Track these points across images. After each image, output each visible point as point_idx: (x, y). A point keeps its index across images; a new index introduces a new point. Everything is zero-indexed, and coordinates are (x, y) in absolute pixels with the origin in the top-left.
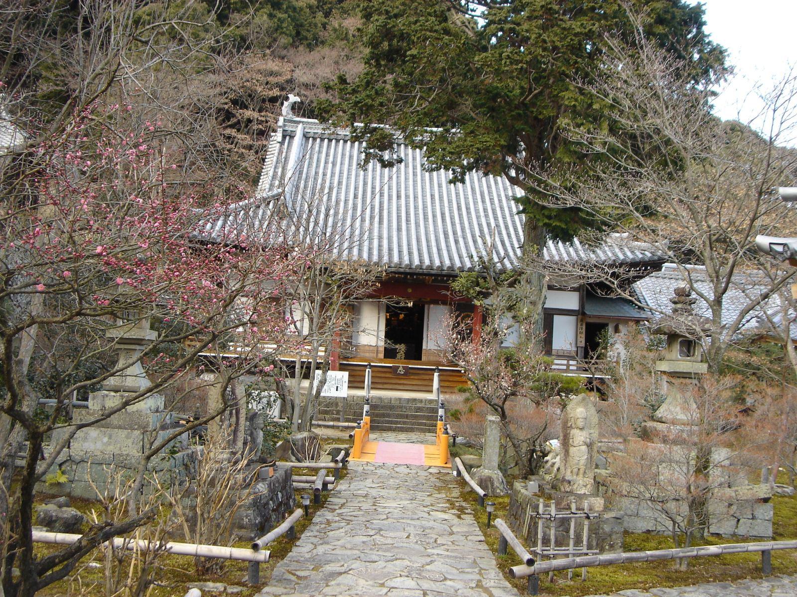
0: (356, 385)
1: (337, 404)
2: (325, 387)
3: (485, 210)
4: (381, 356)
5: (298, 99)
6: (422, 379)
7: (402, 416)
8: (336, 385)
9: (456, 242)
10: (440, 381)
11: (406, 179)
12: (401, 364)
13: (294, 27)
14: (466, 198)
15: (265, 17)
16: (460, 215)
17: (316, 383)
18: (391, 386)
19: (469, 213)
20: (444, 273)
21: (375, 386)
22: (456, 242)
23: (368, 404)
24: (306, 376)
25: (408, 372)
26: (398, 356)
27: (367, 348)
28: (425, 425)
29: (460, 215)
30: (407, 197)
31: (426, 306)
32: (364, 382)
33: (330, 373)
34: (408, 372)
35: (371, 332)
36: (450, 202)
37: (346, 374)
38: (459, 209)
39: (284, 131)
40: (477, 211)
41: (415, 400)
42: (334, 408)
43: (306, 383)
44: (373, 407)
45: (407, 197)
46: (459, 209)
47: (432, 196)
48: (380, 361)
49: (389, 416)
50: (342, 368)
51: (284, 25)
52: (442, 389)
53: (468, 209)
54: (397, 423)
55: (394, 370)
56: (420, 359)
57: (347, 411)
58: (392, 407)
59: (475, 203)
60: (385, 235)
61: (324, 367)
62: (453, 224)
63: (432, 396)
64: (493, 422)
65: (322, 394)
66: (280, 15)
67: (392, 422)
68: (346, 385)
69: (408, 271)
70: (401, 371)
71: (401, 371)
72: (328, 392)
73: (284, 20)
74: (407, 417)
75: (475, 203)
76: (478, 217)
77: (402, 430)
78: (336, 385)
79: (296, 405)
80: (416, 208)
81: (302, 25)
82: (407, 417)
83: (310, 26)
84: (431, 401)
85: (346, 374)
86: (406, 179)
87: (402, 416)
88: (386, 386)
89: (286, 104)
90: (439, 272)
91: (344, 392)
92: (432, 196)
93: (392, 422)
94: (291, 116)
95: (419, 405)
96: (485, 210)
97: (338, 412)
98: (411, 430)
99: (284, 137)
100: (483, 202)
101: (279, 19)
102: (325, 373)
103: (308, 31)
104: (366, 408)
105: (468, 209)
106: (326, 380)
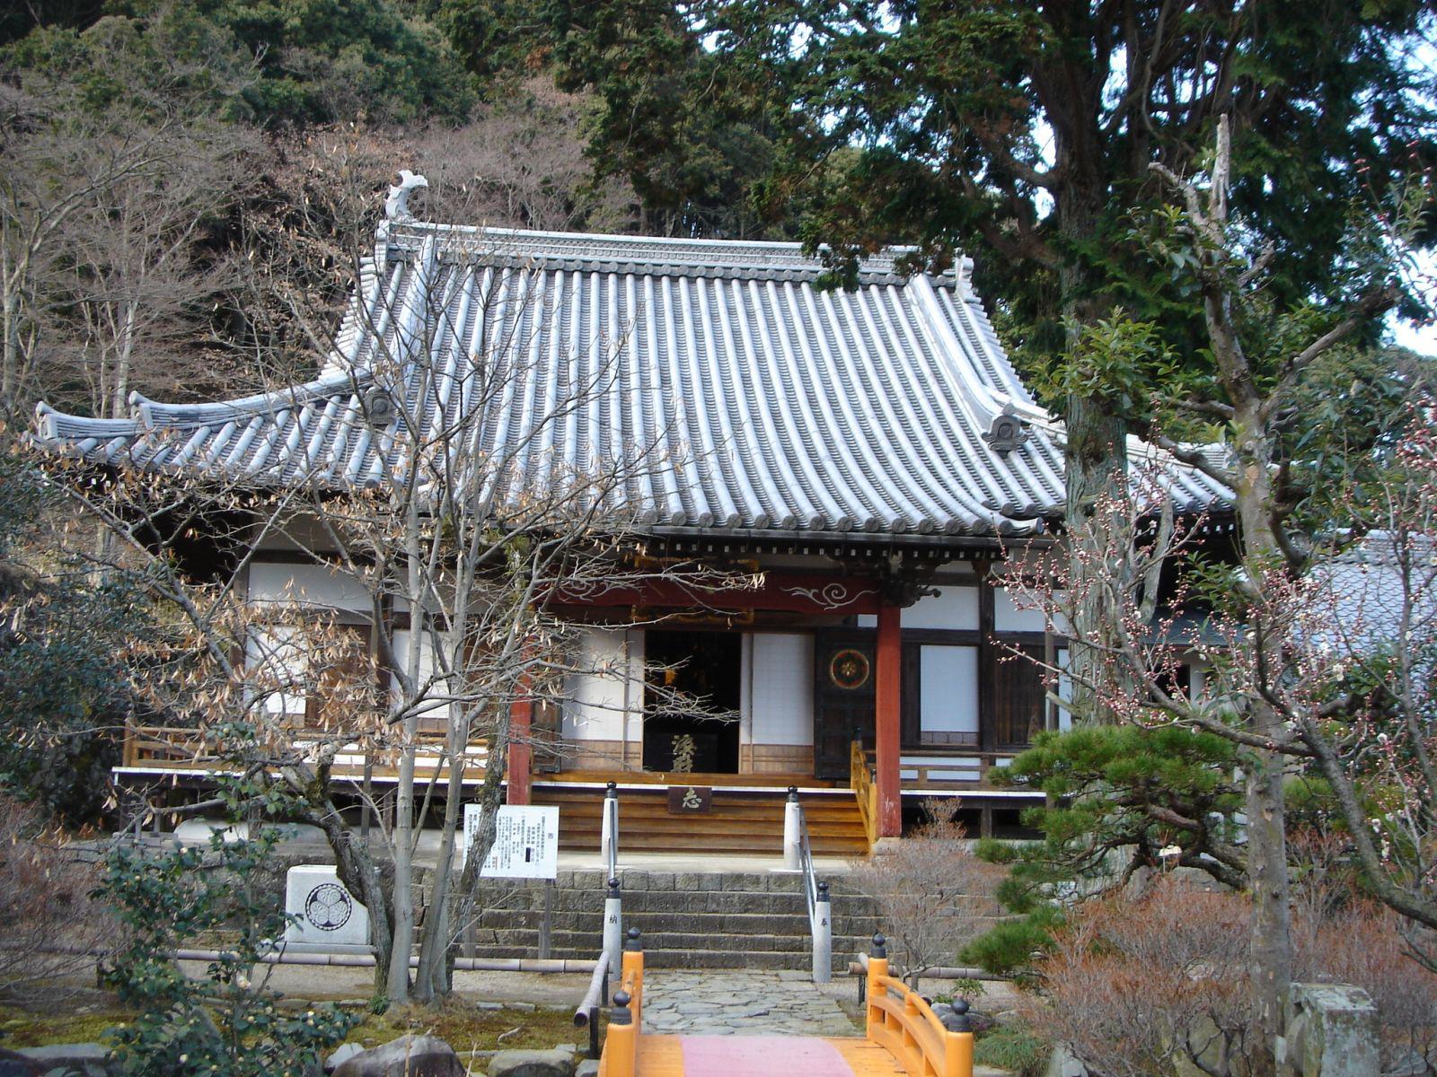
0: (577, 841)
1: (528, 901)
2: (495, 851)
3: (875, 406)
4: (637, 764)
5: (421, 180)
6: (752, 820)
7: (708, 924)
8: (526, 845)
9: (820, 471)
10: (806, 823)
11: (680, 345)
12: (692, 787)
13: (419, 87)
14: (826, 382)
15: (358, 59)
16: (818, 417)
17: (464, 842)
18: (733, 844)
19: (836, 411)
20: (804, 535)
21: (627, 841)
22: (820, 471)
23: (616, 895)
24: (434, 822)
25: (712, 805)
26: (677, 764)
27: (601, 748)
28: (772, 945)
29: (818, 417)
30: (685, 380)
31: (745, 638)
32: (599, 833)
33: (504, 811)
34: (712, 805)
35: (610, 708)
36: (788, 389)
37: (551, 814)
38: (813, 402)
39: (390, 250)
40: (856, 408)
41: (738, 878)
42: (520, 908)
43: (432, 841)
44: (630, 903)
45: (685, 380)
46: (813, 402)
47: (745, 379)
48: (637, 778)
49: (671, 924)
50: (540, 797)
51: (400, 78)
52: (813, 843)
53: (833, 403)
54: (694, 943)
55: (675, 797)
56: (736, 771)
57: (560, 921)
58: (678, 901)
59: (849, 391)
60: (653, 359)
61: (494, 796)
62: (804, 435)
63: (783, 865)
64: (1346, 1018)
65: (486, 872)
66: (389, 58)
67: (679, 943)
68: (553, 843)
69: (708, 531)
70: (692, 800)
71: (692, 800)
72: (502, 865)
73: (398, 68)
74: (721, 925)
75: (849, 391)
76: (861, 420)
77: (712, 964)
78: (526, 845)
79: (399, 917)
80: (709, 403)
81: (436, 85)
82: (721, 925)
83: (454, 86)
84: (782, 879)
85: (551, 814)
86: (680, 345)
87: (708, 924)
88: (707, 844)
89: (394, 191)
90: (791, 534)
91: (549, 864)
92: (745, 379)
93: (679, 943)
94: (405, 217)
95: (751, 891)
96: (875, 406)
97: (532, 920)
98: (734, 963)
99: (391, 265)
100: (868, 388)
101: (388, 67)
102: (490, 811)
103: (449, 96)
104: (611, 908)
105: (833, 403)
106: (493, 832)
